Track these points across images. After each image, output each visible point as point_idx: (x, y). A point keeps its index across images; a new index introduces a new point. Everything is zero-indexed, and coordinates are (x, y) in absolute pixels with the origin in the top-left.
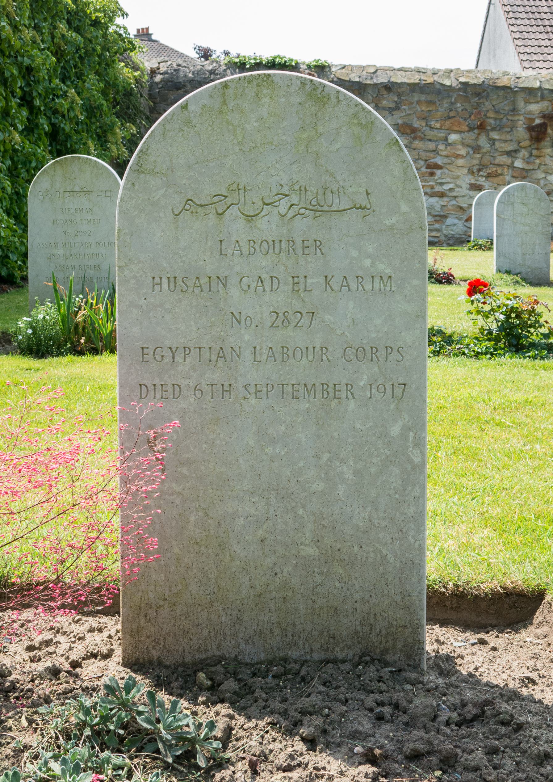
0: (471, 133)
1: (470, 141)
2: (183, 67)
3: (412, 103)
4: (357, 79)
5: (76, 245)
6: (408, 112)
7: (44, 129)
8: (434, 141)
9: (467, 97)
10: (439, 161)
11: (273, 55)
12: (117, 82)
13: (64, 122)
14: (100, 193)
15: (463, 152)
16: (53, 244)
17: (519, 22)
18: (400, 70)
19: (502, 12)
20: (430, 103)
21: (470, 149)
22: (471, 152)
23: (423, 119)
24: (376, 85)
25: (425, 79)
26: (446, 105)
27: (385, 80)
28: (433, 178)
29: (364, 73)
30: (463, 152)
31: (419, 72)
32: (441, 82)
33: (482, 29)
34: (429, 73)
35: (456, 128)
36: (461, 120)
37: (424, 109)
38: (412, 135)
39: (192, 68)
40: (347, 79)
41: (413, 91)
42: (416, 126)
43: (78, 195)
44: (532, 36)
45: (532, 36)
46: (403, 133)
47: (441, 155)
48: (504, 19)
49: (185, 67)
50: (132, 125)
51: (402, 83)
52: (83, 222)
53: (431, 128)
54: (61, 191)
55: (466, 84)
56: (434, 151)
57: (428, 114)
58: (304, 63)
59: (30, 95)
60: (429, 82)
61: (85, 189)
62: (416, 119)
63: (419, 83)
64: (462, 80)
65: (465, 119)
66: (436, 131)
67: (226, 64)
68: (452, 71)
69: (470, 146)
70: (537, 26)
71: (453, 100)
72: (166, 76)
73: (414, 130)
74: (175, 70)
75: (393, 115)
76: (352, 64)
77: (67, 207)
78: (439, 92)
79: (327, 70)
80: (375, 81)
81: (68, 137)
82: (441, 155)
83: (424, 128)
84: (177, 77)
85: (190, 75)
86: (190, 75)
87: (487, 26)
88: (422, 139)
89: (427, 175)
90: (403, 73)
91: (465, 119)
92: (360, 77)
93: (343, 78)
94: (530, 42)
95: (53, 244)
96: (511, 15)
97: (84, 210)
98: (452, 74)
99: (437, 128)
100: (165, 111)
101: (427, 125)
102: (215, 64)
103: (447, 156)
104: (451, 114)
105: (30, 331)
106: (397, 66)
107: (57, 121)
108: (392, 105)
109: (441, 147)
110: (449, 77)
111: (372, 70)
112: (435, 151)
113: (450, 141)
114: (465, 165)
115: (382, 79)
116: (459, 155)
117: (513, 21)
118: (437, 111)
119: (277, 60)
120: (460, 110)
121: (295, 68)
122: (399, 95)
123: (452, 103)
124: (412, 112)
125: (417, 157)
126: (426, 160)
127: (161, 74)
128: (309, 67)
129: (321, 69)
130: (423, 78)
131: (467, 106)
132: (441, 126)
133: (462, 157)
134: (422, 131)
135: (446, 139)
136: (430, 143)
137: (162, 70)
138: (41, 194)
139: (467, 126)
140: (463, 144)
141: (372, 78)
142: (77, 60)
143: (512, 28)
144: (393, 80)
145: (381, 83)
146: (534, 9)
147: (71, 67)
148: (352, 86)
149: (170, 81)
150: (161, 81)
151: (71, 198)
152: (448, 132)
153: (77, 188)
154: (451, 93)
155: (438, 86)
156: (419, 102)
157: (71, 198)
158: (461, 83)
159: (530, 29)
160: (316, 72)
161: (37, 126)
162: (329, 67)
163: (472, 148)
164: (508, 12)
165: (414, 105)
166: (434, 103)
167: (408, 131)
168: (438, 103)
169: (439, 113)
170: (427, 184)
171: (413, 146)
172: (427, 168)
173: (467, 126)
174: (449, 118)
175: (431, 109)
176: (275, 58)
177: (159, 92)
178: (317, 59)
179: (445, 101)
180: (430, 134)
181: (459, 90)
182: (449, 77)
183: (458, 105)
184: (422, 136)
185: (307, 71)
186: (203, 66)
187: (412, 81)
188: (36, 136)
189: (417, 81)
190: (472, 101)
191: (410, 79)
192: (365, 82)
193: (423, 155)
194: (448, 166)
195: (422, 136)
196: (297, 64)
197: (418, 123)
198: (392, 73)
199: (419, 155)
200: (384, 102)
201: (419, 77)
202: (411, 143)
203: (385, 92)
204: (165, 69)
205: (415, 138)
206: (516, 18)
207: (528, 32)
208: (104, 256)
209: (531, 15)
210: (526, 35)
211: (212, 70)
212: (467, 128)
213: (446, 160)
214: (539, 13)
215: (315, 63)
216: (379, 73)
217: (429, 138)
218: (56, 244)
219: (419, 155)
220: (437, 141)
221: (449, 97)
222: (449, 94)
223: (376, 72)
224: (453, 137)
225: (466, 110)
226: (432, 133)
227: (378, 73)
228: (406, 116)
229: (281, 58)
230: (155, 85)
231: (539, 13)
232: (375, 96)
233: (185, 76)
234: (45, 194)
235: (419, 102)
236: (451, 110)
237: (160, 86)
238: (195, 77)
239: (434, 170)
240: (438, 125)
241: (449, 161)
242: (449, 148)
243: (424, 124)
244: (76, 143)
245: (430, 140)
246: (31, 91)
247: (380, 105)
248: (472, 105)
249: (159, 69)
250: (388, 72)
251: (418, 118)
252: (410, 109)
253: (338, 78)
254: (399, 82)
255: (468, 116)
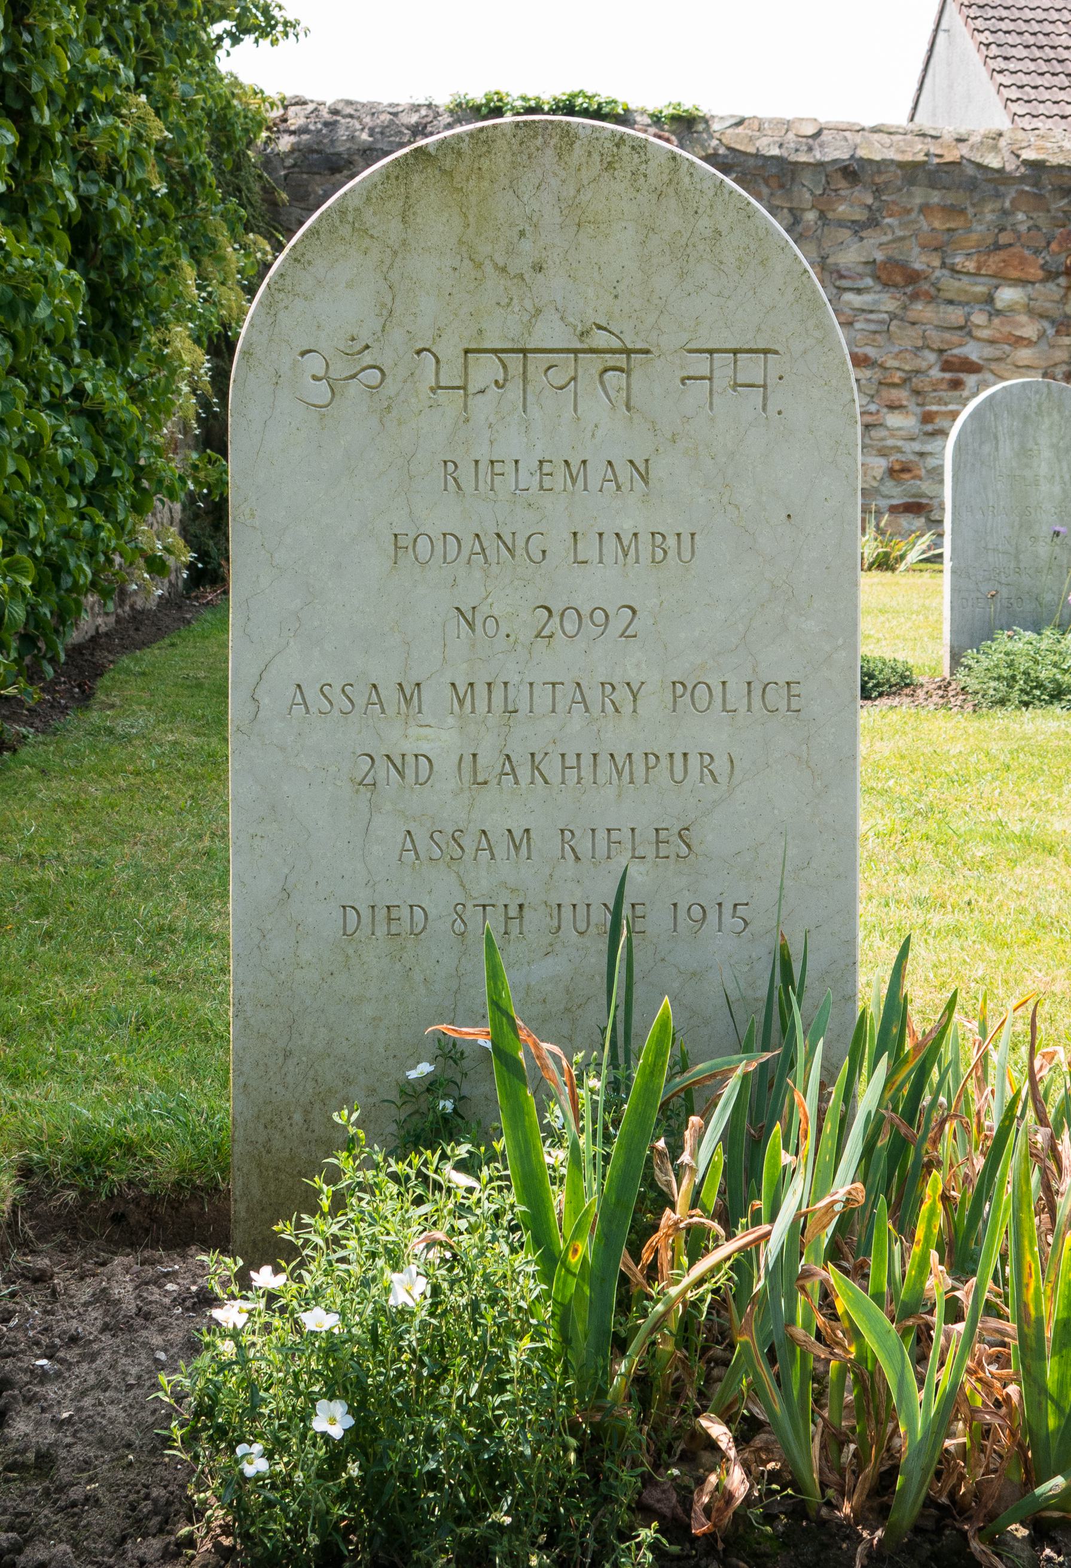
0: (1051, 285)
1: (1048, 305)
2: (345, 117)
3: (909, 211)
4: (775, 151)
5: (543, 696)
6: (901, 234)
7: (63, 208)
8: (960, 303)
9: (1039, 197)
10: (973, 352)
11: (568, 92)
12: (230, 113)
13: (115, 195)
14: (700, 365)
15: (1030, 330)
16: (390, 693)
17: (1012, 65)
18: (876, 130)
19: (971, 46)
20: (952, 211)
21: (1046, 324)
22: (1051, 332)
23: (936, 249)
24: (821, 164)
25: (939, 152)
26: (989, 217)
27: (842, 154)
28: (957, 393)
29: (791, 136)
30: (1030, 330)
31: (924, 135)
32: (979, 160)
33: (916, 86)
34: (948, 138)
35: (1015, 274)
36: (1027, 252)
37: (937, 224)
38: (909, 290)
39: (367, 120)
40: (751, 150)
41: (911, 181)
42: (917, 266)
43: (558, 377)
44: (1046, 95)
45: (1046, 95)
46: (886, 285)
47: (978, 339)
48: (978, 59)
49: (351, 116)
50: (260, 239)
51: (884, 160)
52: (588, 549)
53: (954, 271)
54: (450, 349)
55: (1037, 166)
56: (961, 328)
57: (946, 237)
58: (643, 112)
59: (18, 89)
60: (948, 158)
61: (601, 339)
62: (917, 250)
63: (925, 163)
64: (1026, 155)
65: (1037, 252)
66: (965, 279)
67: (451, 111)
68: (1000, 135)
69: (1047, 317)
70: (1053, 74)
71: (1007, 204)
72: (305, 137)
73: (913, 277)
74: (326, 124)
75: (862, 239)
76: (760, 116)
77: (483, 453)
78: (972, 186)
79: (701, 127)
80: (818, 156)
81: (123, 245)
82: (978, 339)
83: (938, 273)
84: (332, 141)
85: (365, 136)
86: (365, 136)
87: (927, 80)
88: (931, 299)
89: (944, 386)
90: (885, 139)
91: (1037, 252)
92: (781, 146)
93: (742, 148)
94: (1042, 109)
95: (390, 693)
96: (994, 50)
97: (596, 472)
98: (1003, 143)
99: (968, 273)
100: (301, 223)
101: (944, 265)
102: (423, 112)
103: (992, 342)
104: (1003, 239)
105: (332, 1420)
106: (868, 123)
107: (94, 190)
108: (860, 215)
109: (979, 318)
110: (995, 148)
111: (810, 130)
112: (965, 329)
113: (999, 305)
114: (1036, 363)
115: (835, 152)
116: (1021, 338)
117: (1000, 64)
118: (969, 230)
119: (580, 100)
120: (1023, 228)
121: (624, 119)
122: (878, 192)
123: (1005, 212)
124: (907, 233)
125: (920, 343)
126: (941, 351)
127: (292, 133)
128: (657, 119)
129: (685, 125)
130: (933, 150)
131: (1042, 219)
132: (979, 268)
133: (1029, 343)
134: (933, 278)
135: (990, 299)
136: (950, 308)
137: (294, 123)
138: (314, 364)
139: (1042, 267)
140: (1030, 312)
141: (810, 149)
142: (142, 19)
143: (1000, 78)
144: (862, 153)
145: (835, 161)
146: (1042, 40)
147: (127, 40)
148: (763, 166)
149: (312, 151)
150: (292, 151)
151: (514, 391)
152: (995, 281)
153: (550, 333)
154: (1002, 188)
155: (970, 171)
156: (924, 209)
157: (514, 391)
158: (1025, 162)
159: (1039, 81)
160: (673, 132)
161: (37, 193)
162: (705, 120)
163: (1053, 322)
164: (988, 45)
165: (914, 215)
166: (963, 211)
167: (899, 279)
168: (971, 211)
169: (974, 236)
170: (943, 408)
171: (911, 315)
172: (943, 370)
173: (1042, 267)
174: (997, 247)
175: (952, 225)
176: (574, 96)
177: (286, 176)
178: (675, 101)
179: (988, 207)
180: (951, 286)
181: (1022, 179)
182: (995, 148)
183: (1021, 216)
184: (933, 291)
185: (653, 130)
186: (395, 114)
187: (908, 157)
188: (36, 227)
189: (921, 157)
190: (1053, 206)
191: (903, 152)
192: (793, 158)
193: (936, 338)
194: (993, 366)
195: (933, 291)
196: (626, 110)
197: (924, 259)
198: (858, 138)
199: (924, 337)
200: (841, 208)
201: (925, 148)
202: (905, 308)
203: (843, 184)
204: (301, 121)
205: (915, 297)
206: (1006, 58)
207: (1036, 87)
208: (720, 765)
209: (1037, 53)
210: (1033, 94)
211: (417, 124)
212: (1041, 274)
213: (989, 351)
214: (1052, 47)
215: (671, 111)
216: (826, 136)
217: (949, 295)
218: (410, 694)
219: (924, 337)
220: (967, 303)
221: (998, 196)
222: (997, 191)
223: (818, 134)
224: (1007, 295)
225: (1038, 228)
226: (957, 284)
227: (823, 138)
228: (893, 241)
229: (589, 98)
230: (276, 162)
231: (1052, 47)
232: (819, 192)
233: (352, 138)
234: (340, 369)
235: (924, 209)
236: (1002, 229)
237: (289, 162)
238: (375, 141)
239: (962, 375)
240: (971, 266)
241: (998, 354)
242: (996, 321)
243: (937, 263)
244: (144, 266)
245: (951, 302)
246: (25, 75)
247: (830, 215)
248: (1054, 218)
249: (285, 121)
250: (847, 134)
251: (923, 247)
252: (903, 225)
253: (729, 148)
254: (878, 158)
255: (1044, 244)
